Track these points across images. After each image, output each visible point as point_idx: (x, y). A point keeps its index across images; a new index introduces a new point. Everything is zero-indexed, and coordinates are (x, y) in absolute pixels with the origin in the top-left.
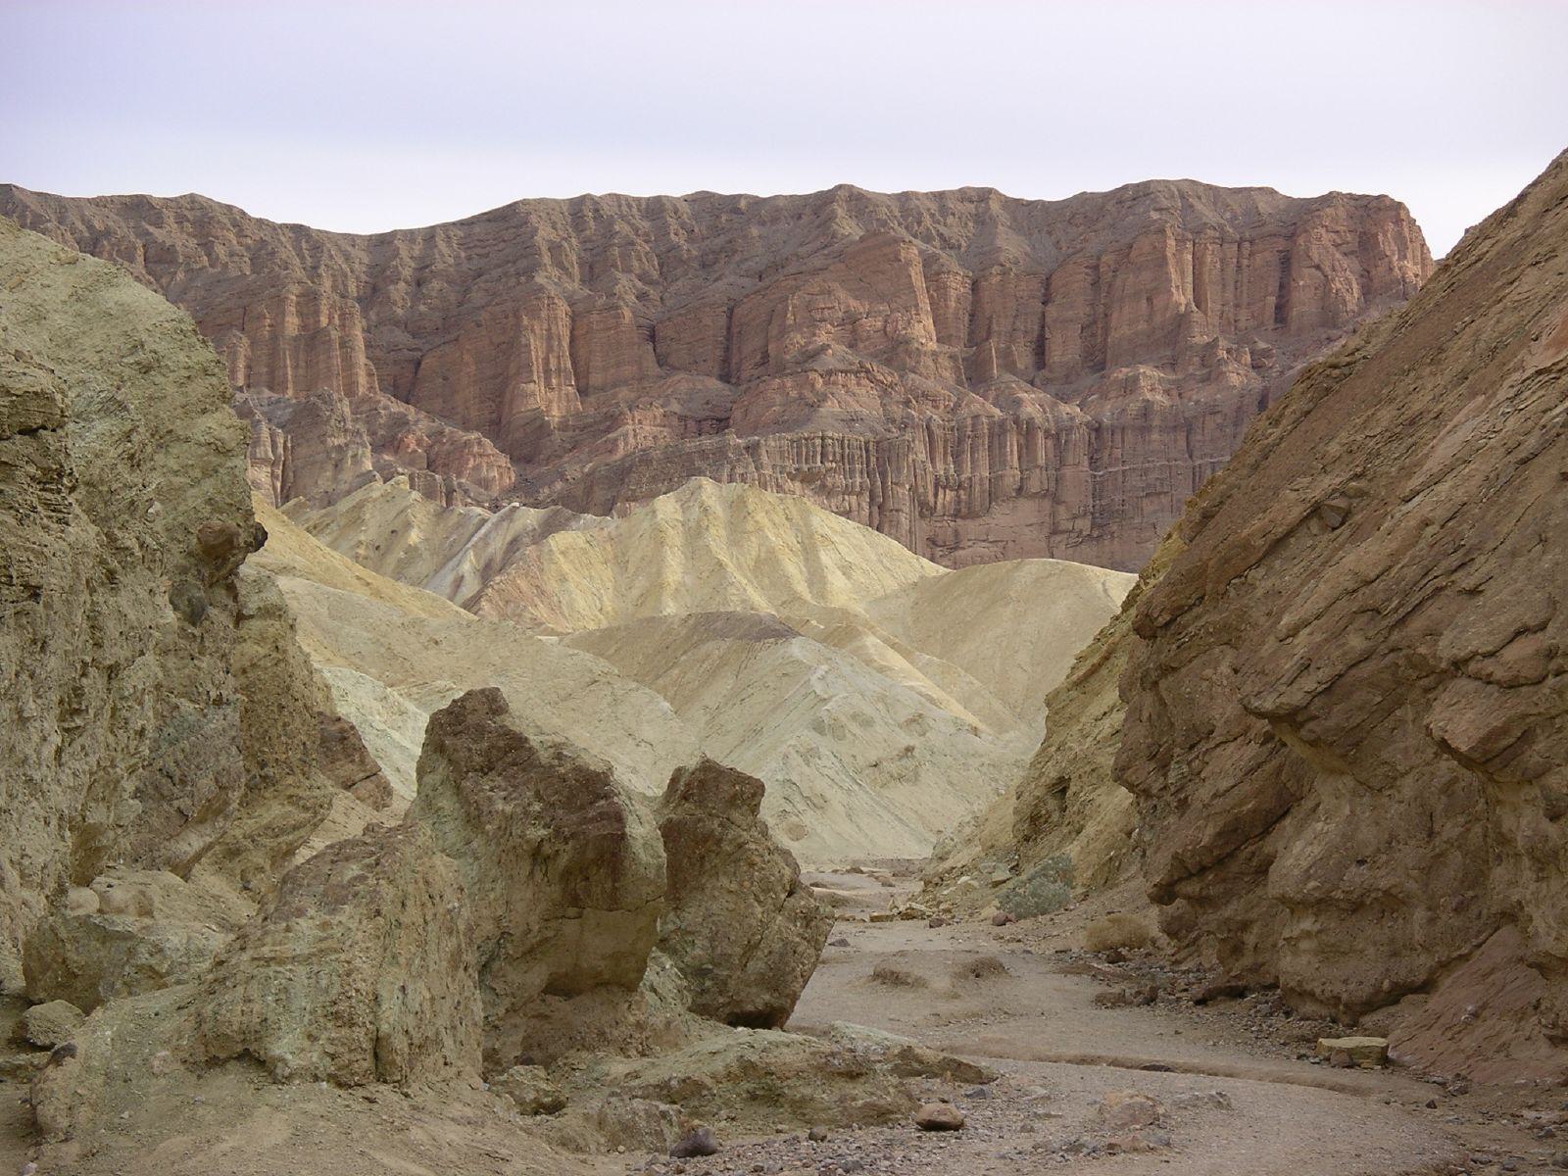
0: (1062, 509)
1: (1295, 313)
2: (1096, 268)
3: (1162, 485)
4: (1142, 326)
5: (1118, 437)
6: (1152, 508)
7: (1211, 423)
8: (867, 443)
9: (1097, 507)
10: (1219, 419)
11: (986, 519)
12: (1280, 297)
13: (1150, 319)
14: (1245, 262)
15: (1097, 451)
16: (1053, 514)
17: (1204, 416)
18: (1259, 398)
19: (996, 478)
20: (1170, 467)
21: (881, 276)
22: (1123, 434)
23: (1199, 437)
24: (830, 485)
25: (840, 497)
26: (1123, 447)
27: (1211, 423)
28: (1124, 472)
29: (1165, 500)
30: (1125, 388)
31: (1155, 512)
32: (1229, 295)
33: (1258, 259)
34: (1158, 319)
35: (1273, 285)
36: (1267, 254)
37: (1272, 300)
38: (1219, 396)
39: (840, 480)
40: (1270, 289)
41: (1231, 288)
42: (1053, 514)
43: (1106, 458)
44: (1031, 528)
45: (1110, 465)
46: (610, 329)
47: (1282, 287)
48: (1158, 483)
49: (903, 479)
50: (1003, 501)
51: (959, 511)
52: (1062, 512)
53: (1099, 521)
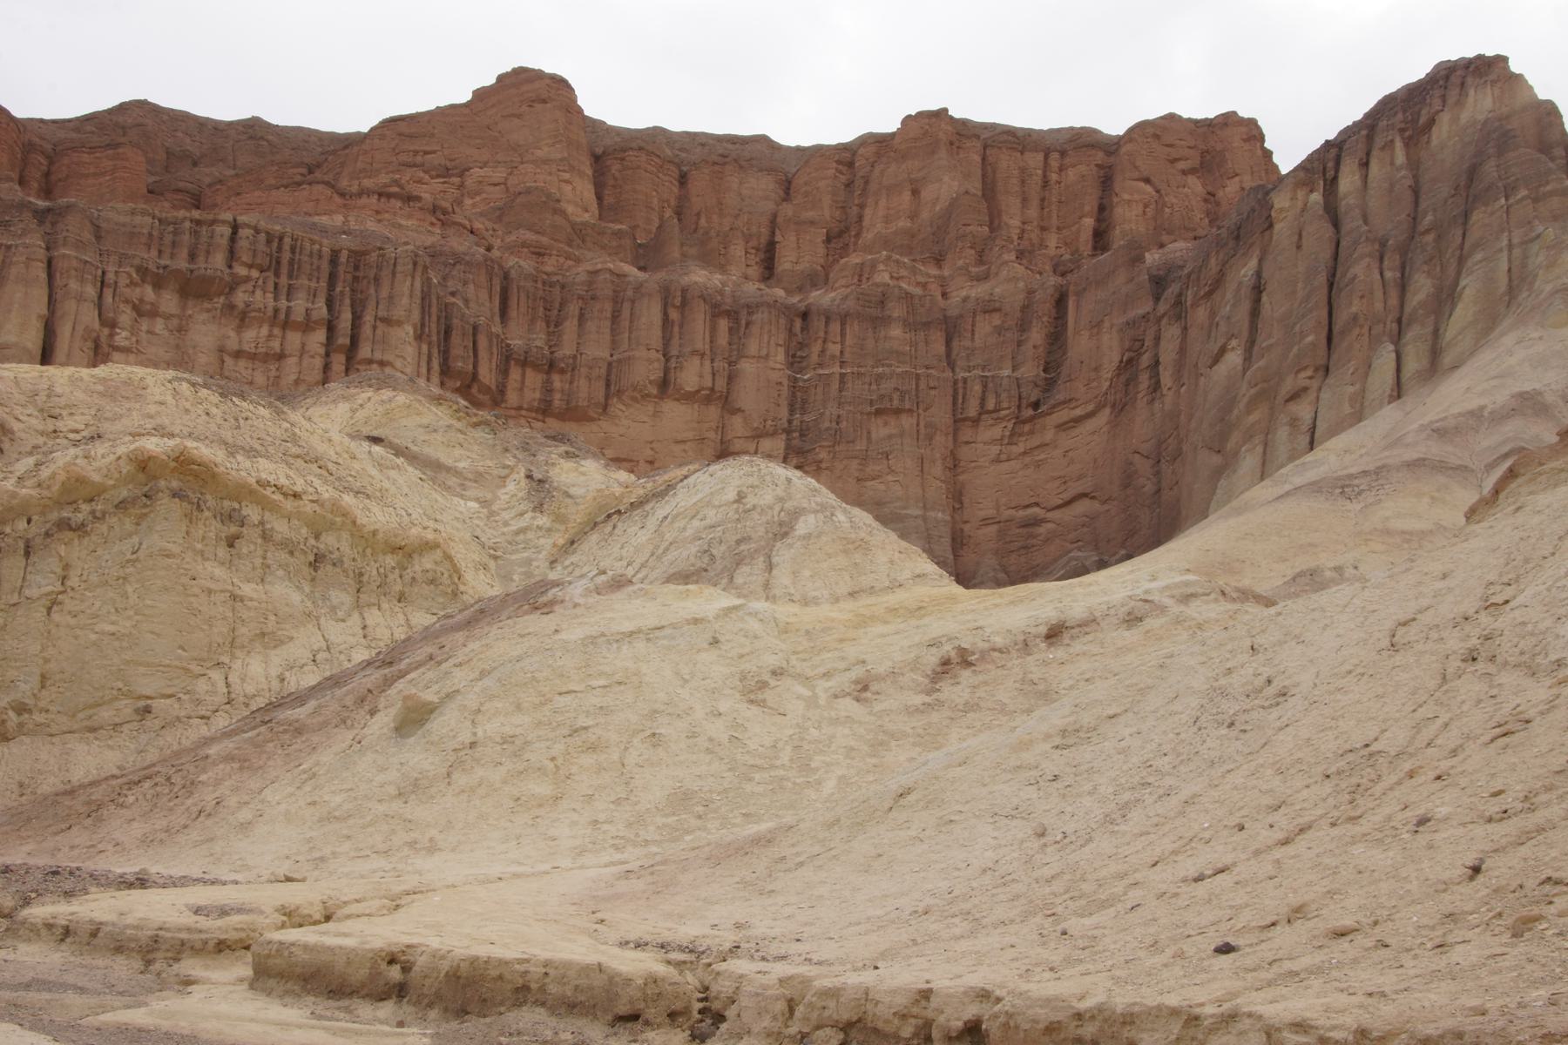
0: (737, 421)
1: (1117, 232)
2: (851, 164)
3: (902, 399)
4: (903, 223)
5: (835, 327)
6: (884, 432)
7: (984, 326)
8: (335, 254)
9: (795, 423)
10: (996, 320)
11: (604, 424)
12: (1098, 221)
13: (913, 216)
14: (1054, 177)
15: (801, 346)
16: (722, 428)
17: (974, 317)
18: (1057, 295)
19: (619, 361)
20: (918, 377)
21: (516, 121)
22: (843, 324)
23: (967, 343)
24: (241, 305)
25: (265, 331)
26: (842, 343)
27: (984, 326)
28: (842, 376)
29: (907, 422)
30: (861, 276)
31: (890, 437)
32: (1033, 212)
33: (1072, 175)
34: (925, 215)
35: (1090, 204)
36: (1083, 168)
37: (1089, 222)
38: (997, 290)
39: (263, 299)
40: (1087, 208)
41: (1035, 203)
42: (722, 428)
43: (814, 358)
44: (682, 446)
45: (821, 365)
46: (103, 174)
47: (1102, 209)
48: (896, 396)
49: (398, 312)
50: (634, 399)
51: (549, 403)
52: (737, 425)
53: (796, 442)
